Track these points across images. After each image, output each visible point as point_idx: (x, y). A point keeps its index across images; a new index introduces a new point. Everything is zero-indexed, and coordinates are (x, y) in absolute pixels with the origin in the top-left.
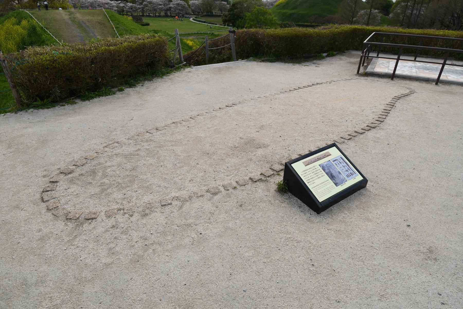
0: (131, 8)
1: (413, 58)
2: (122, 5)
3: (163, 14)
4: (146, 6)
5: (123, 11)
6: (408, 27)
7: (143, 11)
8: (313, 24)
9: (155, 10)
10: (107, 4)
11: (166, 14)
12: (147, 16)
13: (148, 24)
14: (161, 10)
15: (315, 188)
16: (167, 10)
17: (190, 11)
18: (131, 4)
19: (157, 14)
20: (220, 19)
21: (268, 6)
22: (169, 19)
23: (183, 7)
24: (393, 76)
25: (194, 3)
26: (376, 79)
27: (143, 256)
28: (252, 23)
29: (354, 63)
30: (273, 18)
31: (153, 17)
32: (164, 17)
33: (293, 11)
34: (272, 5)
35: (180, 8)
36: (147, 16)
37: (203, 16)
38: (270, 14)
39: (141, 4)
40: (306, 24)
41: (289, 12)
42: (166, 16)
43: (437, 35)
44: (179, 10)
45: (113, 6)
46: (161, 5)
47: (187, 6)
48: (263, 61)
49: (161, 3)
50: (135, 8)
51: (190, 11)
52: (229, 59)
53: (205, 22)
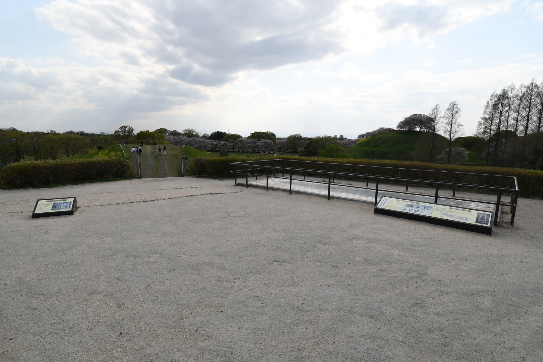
0: (224, 145)
2: (216, 143)
3: (251, 150)
4: (237, 143)
5: (216, 147)
6: (494, 165)
7: (234, 149)
9: (244, 147)
11: (253, 150)
12: (236, 152)
14: (250, 147)
16: (255, 147)
17: (276, 148)
23: (270, 145)
24: (247, 186)
26: (300, 195)
29: (288, 183)
32: (251, 152)
33: (374, 149)
34: (355, 143)
36: (236, 152)
39: (233, 142)
43: (459, 171)
45: (208, 144)
48: (197, 177)
50: (227, 145)
51: (276, 148)
52: (166, 176)
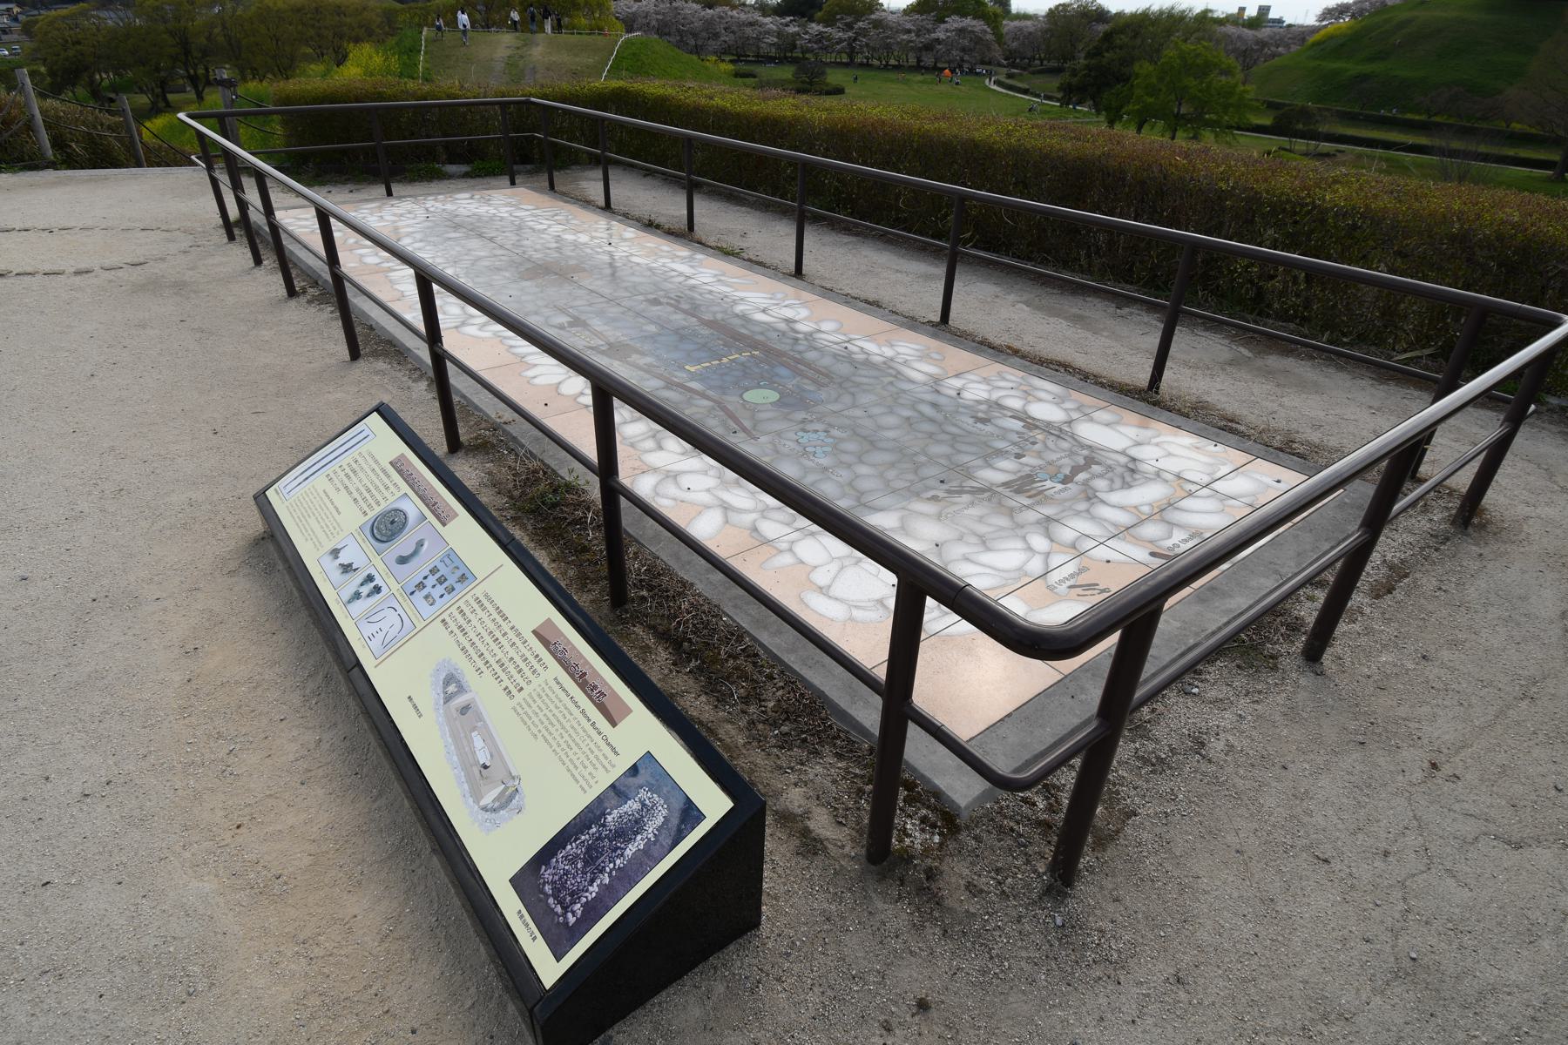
0: (820, 37)
1: (671, 205)
2: (793, 29)
8: (1438, 119)
9: (888, 47)
10: (751, 24)
11: (919, 61)
13: (839, 91)
14: (906, 47)
15: (562, 695)
16: (928, 47)
17: (997, 53)
18: (820, 28)
19: (892, 62)
20: (1054, 83)
21: (1287, 46)
22: (920, 78)
23: (978, 40)
25: (1020, 29)
27: (644, 805)
28: (1150, 100)
30: (1236, 85)
31: (878, 68)
33: (1368, 68)
35: (966, 42)
37: (1040, 72)
38: (1227, 72)
39: (849, 26)
40: (1409, 116)
41: (1352, 68)
42: (918, 68)
44: (963, 50)
45: (768, 32)
46: (909, 31)
47: (989, 37)
49: (909, 26)
50: (829, 39)
51: (997, 53)
53: (1026, 92)
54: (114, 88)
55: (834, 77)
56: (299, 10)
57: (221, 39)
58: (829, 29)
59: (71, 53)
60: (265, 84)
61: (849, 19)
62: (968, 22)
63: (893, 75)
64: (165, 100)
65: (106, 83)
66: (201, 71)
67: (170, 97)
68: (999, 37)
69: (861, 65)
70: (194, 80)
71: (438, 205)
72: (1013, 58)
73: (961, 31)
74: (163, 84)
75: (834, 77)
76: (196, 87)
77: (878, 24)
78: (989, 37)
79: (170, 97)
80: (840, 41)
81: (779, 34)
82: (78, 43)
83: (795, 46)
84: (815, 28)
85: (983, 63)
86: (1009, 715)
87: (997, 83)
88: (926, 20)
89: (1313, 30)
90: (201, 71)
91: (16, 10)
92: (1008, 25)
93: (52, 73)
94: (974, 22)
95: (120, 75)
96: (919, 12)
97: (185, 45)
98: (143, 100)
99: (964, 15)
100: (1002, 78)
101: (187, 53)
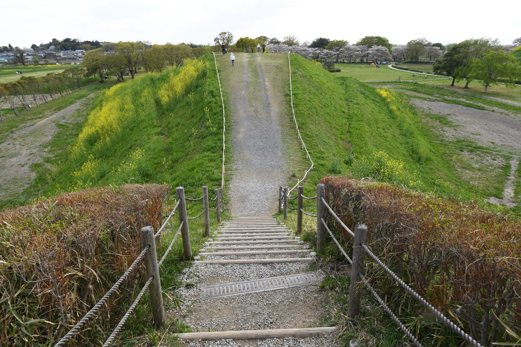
0: (327, 54)
2: (318, 52)
10: (304, 51)
13: (339, 71)
14: (357, 56)
17: (391, 58)
18: (327, 51)
20: (431, 67)
23: (383, 53)
31: (347, 63)
35: (380, 54)
37: (405, 63)
39: (338, 50)
42: (362, 62)
44: (378, 56)
46: (358, 51)
47: (388, 52)
49: (358, 49)
54: (107, 74)
55: (337, 66)
56: (166, 49)
57: (141, 59)
58: (330, 51)
59: (94, 63)
60: (153, 73)
61: (337, 48)
62: (380, 47)
63: (352, 65)
64: (122, 78)
65: (104, 73)
66: (134, 69)
67: (124, 77)
68: (390, 51)
69: (341, 62)
70: (131, 72)
71: (242, 130)
72: (395, 58)
73: (378, 50)
74: (122, 73)
75: (337, 66)
76: (132, 74)
77: (348, 49)
78: (388, 52)
79: (124, 77)
80: (335, 55)
81: (313, 54)
82: (97, 60)
83: (318, 57)
84: (325, 51)
85: (386, 60)
86: (96, 44)
87: (393, 66)
88: (365, 47)
89: (511, 47)
90: (134, 69)
91: (84, 51)
92: (393, 48)
93: (88, 70)
94: (382, 47)
95: (110, 70)
96: (362, 45)
97: (130, 61)
98: (115, 78)
99: (378, 45)
100: (394, 65)
101: (130, 63)
